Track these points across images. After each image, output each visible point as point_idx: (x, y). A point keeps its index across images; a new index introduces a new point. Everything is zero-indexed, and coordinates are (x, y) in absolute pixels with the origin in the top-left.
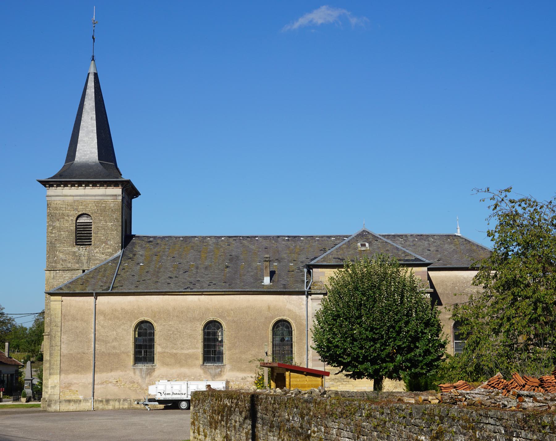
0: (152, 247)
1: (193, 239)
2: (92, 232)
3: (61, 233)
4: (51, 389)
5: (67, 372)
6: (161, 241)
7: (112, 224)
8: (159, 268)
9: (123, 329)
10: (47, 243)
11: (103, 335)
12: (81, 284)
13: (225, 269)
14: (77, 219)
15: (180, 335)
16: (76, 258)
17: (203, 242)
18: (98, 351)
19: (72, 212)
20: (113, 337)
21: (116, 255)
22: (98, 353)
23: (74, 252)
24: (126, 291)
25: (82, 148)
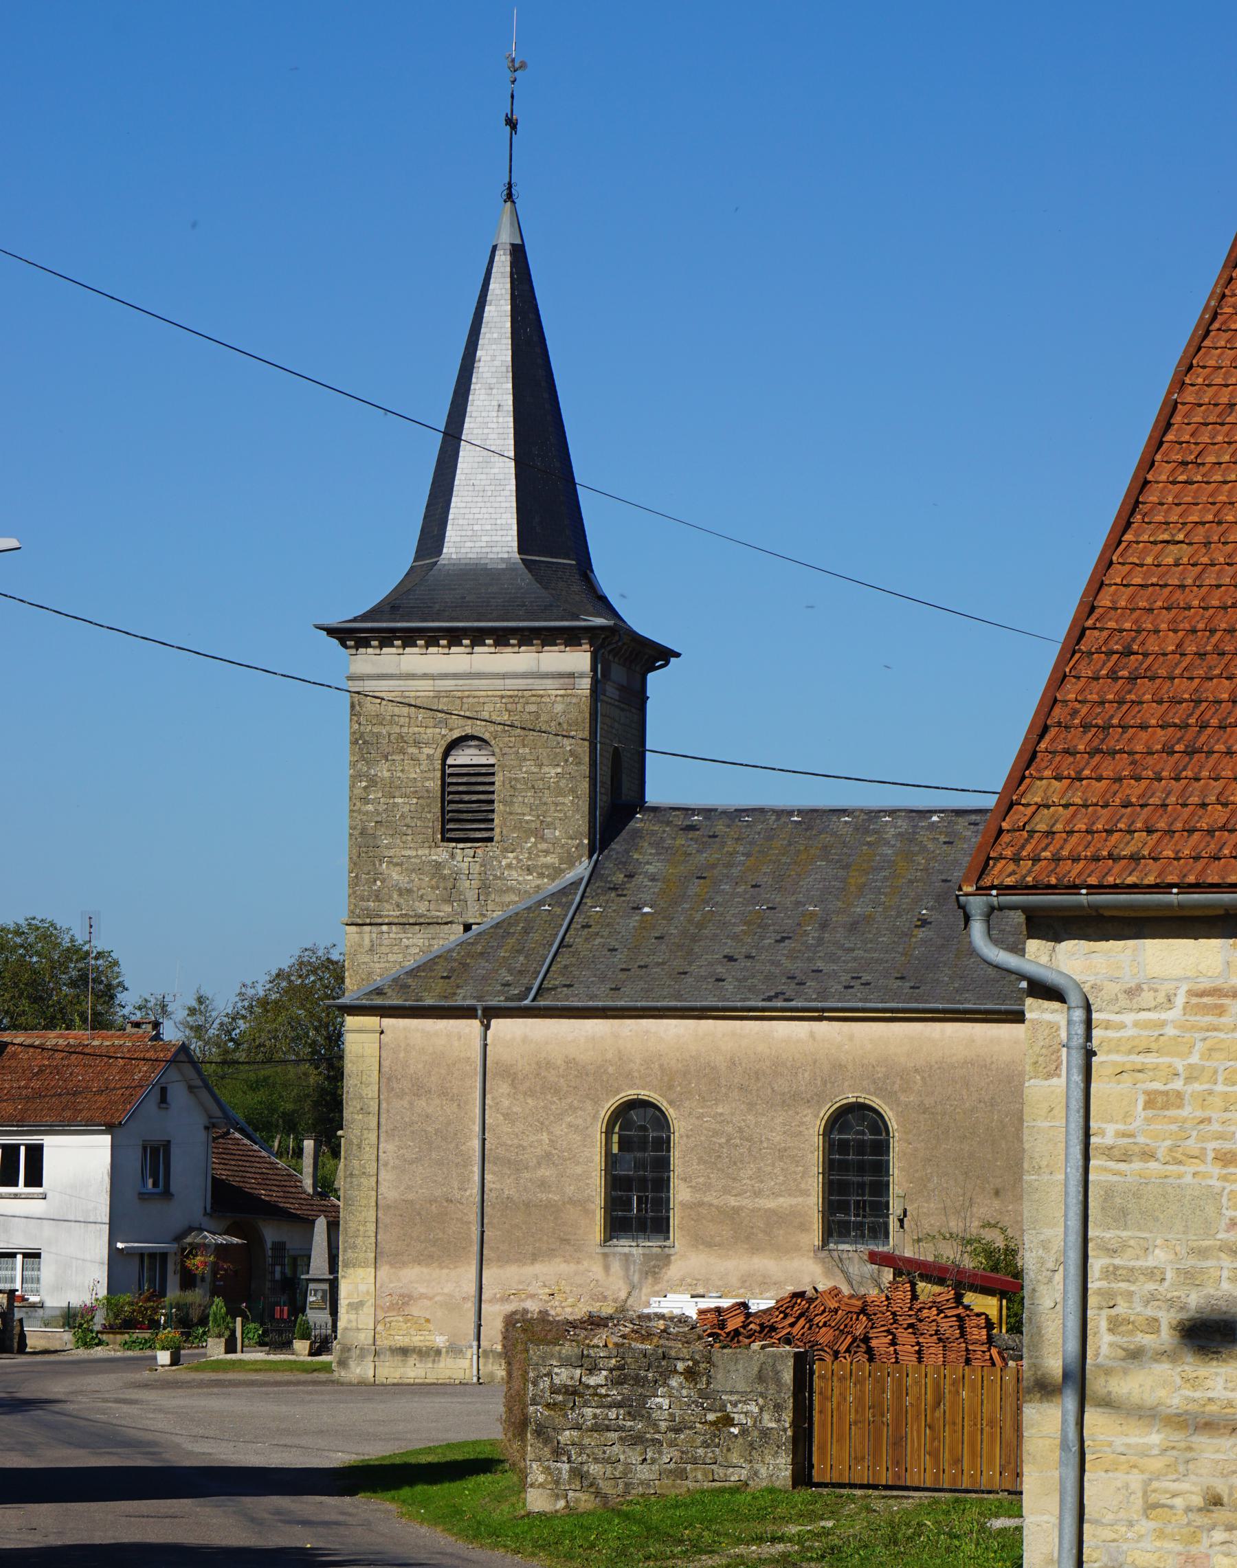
0: (693, 849)
1: (835, 819)
2: (495, 797)
3: (396, 800)
4: (347, 1313)
5: (398, 1260)
6: (729, 826)
7: (559, 770)
8: (701, 926)
9: (570, 1125)
10: (351, 835)
11: (509, 1142)
12: (443, 977)
13: (916, 932)
14: (446, 754)
15: (750, 1150)
16: (442, 885)
17: (867, 831)
18: (493, 1195)
19: (429, 731)
20: (539, 1152)
21: (571, 876)
22: (494, 1200)
23: (438, 865)
24: (579, 1004)
25: (467, 511)
